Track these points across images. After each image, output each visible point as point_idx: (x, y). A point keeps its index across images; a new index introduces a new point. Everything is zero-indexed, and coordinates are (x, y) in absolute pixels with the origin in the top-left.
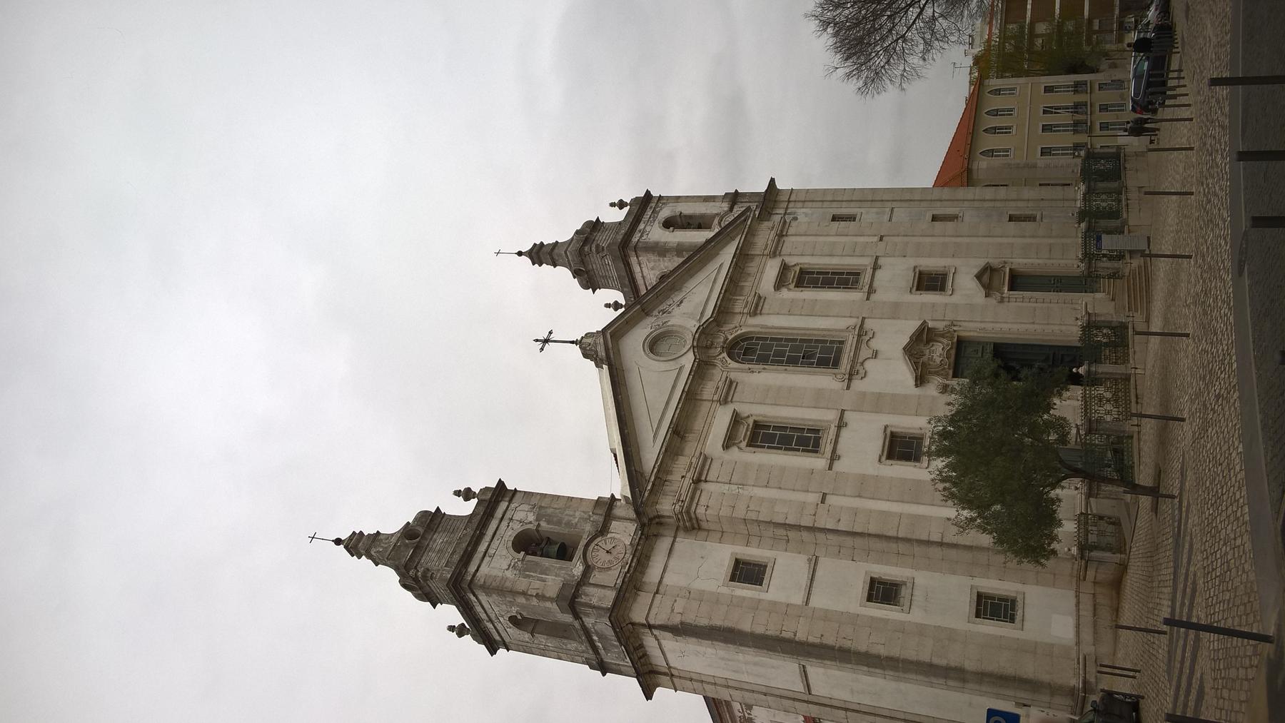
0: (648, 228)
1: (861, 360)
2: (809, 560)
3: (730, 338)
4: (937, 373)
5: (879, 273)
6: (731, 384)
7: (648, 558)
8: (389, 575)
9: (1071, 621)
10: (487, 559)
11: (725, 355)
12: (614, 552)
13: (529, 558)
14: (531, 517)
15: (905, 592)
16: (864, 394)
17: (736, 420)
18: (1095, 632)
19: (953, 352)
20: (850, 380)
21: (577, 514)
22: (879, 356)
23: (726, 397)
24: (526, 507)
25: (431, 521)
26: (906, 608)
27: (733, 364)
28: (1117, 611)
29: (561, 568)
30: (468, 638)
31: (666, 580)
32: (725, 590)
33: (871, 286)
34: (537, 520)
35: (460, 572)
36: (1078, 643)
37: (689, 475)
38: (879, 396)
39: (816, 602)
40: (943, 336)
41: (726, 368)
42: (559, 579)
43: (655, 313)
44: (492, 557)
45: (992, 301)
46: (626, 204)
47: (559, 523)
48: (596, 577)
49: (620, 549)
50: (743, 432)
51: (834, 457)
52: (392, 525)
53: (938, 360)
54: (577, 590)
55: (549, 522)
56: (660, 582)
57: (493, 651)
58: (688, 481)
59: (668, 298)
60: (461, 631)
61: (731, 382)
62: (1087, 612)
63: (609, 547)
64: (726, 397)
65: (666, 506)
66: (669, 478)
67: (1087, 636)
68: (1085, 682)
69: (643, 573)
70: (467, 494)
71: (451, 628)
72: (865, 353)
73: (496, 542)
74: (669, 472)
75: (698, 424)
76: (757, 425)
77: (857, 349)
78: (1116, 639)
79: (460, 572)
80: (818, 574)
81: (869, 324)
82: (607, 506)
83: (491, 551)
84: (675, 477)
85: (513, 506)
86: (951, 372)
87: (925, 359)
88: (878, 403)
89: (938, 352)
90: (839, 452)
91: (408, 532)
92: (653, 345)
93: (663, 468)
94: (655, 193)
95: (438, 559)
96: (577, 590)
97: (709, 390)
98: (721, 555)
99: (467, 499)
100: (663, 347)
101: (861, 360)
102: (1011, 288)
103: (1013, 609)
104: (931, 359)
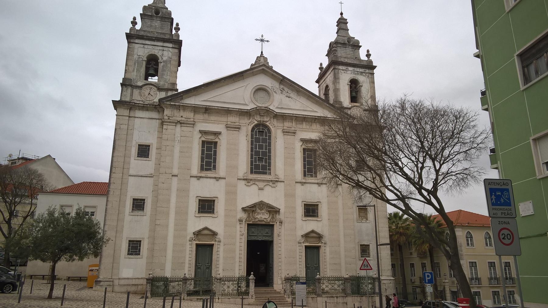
0: (349, 72)
1: (256, 183)
2: (151, 174)
3: (267, 124)
4: (249, 217)
5: (316, 186)
6: (238, 128)
7: (147, 110)
8: (333, 37)
9: (130, 276)
10: (142, 46)
11: (256, 122)
12: (150, 96)
13: (144, 63)
14: (165, 59)
15: (140, 213)
16: (236, 186)
17: (217, 134)
18: (124, 285)
19: (263, 223)
20: (244, 179)
21: (168, 77)
22: (260, 191)
23: (229, 127)
24: (170, 55)
25: (356, 46)
26: (132, 214)
27: (250, 128)
28: (135, 293)
29: (140, 77)
30: (319, 71)
31: (136, 120)
32: (134, 143)
33: (305, 183)
34: (164, 61)
35: (133, 37)
36: (119, 279)
37: (183, 119)
38: (235, 193)
39: (131, 179)
40: (273, 218)
41: (247, 126)
42: (135, 77)
43: (282, 86)
44: (143, 47)
45: (299, 238)
46: (369, 58)
47: (163, 70)
48: (136, 92)
49: (151, 98)
50: (211, 138)
51: (199, 178)
52: (352, 33)
53: (259, 217)
54: (129, 85)
55: (163, 66)
56: (135, 117)
57: (317, 82)
58: (179, 119)
59: (292, 90)
60: (321, 68)
61: (239, 128)
62: (134, 282)
63: (152, 93)
64: (229, 127)
65: (167, 112)
66: (181, 111)
67: (122, 282)
68: (100, 281)
69: (139, 110)
70: (368, 55)
71: (321, 64)
72: (261, 185)
73: (151, 47)
74: (184, 110)
75: (213, 118)
76: (216, 143)
77: (263, 181)
78: (124, 293)
79: (133, 37)
80: (145, 178)
81: (280, 186)
82: (177, 90)
83: (146, 46)
84: (182, 113)
85: (171, 49)
86: (251, 223)
87: (258, 211)
88: (231, 193)
89: (263, 216)
90: (201, 179)
91: (350, 39)
92: (261, 89)
93: (185, 107)
94: (375, 71)
95: (343, 53)
96: (129, 85)
97: (233, 119)
98: (150, 139)
99: (367, 56)
100: (261, 94)
101: (256, 183)
102: (306, 247)
103: (136, 254)
104: (258, 214)
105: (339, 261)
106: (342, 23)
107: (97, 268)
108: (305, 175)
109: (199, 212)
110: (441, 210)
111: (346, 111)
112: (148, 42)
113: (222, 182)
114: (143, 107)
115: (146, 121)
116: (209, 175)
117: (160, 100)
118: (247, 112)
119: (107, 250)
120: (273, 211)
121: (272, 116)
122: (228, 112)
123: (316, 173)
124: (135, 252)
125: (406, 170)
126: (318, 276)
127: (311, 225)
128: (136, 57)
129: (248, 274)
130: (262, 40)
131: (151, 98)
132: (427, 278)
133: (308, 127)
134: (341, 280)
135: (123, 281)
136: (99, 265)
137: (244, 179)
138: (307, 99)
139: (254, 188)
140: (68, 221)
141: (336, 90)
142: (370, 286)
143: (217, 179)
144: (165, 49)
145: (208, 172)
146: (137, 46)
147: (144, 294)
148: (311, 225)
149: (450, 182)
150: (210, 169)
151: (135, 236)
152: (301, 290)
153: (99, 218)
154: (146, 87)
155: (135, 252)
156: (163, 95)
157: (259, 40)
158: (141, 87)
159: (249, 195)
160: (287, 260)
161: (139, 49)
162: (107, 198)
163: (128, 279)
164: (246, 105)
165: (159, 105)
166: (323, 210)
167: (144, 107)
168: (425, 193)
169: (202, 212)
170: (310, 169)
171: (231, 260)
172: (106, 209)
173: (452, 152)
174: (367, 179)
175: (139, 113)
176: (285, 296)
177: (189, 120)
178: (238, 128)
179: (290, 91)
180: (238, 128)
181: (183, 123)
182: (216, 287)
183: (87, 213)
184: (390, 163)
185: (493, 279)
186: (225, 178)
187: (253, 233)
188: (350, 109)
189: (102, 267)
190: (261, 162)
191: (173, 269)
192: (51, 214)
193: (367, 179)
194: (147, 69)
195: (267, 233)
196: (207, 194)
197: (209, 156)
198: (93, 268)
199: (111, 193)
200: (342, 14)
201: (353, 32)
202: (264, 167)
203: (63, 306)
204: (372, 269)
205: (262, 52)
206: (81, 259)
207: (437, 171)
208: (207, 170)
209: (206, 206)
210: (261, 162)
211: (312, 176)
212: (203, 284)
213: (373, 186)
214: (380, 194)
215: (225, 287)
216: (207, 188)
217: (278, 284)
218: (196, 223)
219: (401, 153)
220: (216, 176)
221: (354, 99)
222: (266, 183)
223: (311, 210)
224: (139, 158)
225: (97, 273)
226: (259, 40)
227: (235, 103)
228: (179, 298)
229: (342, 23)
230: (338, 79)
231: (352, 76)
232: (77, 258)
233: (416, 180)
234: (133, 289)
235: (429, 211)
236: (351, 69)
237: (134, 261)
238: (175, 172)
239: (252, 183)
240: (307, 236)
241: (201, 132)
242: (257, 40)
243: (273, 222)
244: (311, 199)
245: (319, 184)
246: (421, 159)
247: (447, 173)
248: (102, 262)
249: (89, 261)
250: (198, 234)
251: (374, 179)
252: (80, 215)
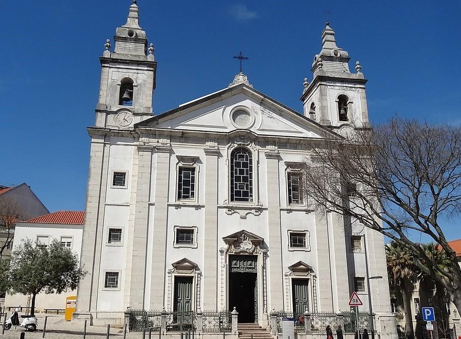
14: (139, 82)
15: (117, 243)
17: (196, 160)
21: (144, 101)
27: (230, 151)
41: (226, 151)
47: (138, 94)
49: (126, 123)
51: (178, 207)
76: (193, 170)
83: (120, 70)
89: (246, 246)
103: (113, 287)
105: (329, 297)
107: (75, 301)
108: (290, 202)
109: (177, 243)
110: (441, 240)
111: (335, 130)
116: (188, 203)
117: (136, 126)
119: (84, 283)
120: (259, 243)
123: (301, 199)
124: (112, 284)
125: (399, 195)
126: (307, 312)
127: (297, 256)
129: (231, 309)
130: (241, 58)
131: (126, 123)
132: (427, 315)
134: (333, 316)
136: (76, 298)
140: (46, 254)
141: (323, 108)
142: (366, 323)
143: (198, 207)
144: (139, 71)
147: (122, 328)
148: (297, 256)
149: (450, 208)
150: (188, 197)
152: (288, 327)
153: (75, 250)
155: (112, 284)
156: (138, 119)
157: (237, 58)
158: (115, 113)
159: (231, 225)
160: (273, 294)
162: (83, 228)
165: (134, 131)
166: (311, 240)
168: (422, 221)
169: (294, 246)
170: (295, 193)
171: (212, 294)
172: (83, 239)
173: (452, 174)
174: (357, 206)
176: (271, 333)
177: (165, 145)
182: (198, 323)
183: (62, 244)
184: (382, 189)
187: (235, 264)
188: (338, 128)
189: (80, 299)
190: (241, 188)
191: (152, 303)
192: (27, 245)
193: (357, 206)
194: (122, 93)
195: (250, 265)
196: (185, 224)
197: (187, 183)
199: (87, 223)
202: (246, 194)
204: (362, 304)
206: (59, 291)
207: (436, 196)
208: (185, 197)
209: (184, 235)
210: (241, 188)
211: (297, 202)
212: (182, 318)
213: (364, 212)
214: (372, 223)
215: (206, 322)
216: (184, 217)
217: (262, 320)
218: (177, 254)
219: (394, 176)
220: (196, 204)
221: (343, 117)
222: (249, 211)
223: (297, 239)
224: (115, 186)
225: (75, 306)
226: (237, 58)
228: (158, 333)
230: (326, 95)
231: (341, 92)
232: (55, 290)
233: (413, 206)
235: (426, 240)
237: (111, 293)
242: (235, 57)
243: (256, 253)
244: (298, 228)
245: (308, 211)
246: (417, 185)
247: (447, 198)
248: (80, 294)
249: (69, 293)
250: (178, 265)
251: (365, 205)
252: (58, 246)
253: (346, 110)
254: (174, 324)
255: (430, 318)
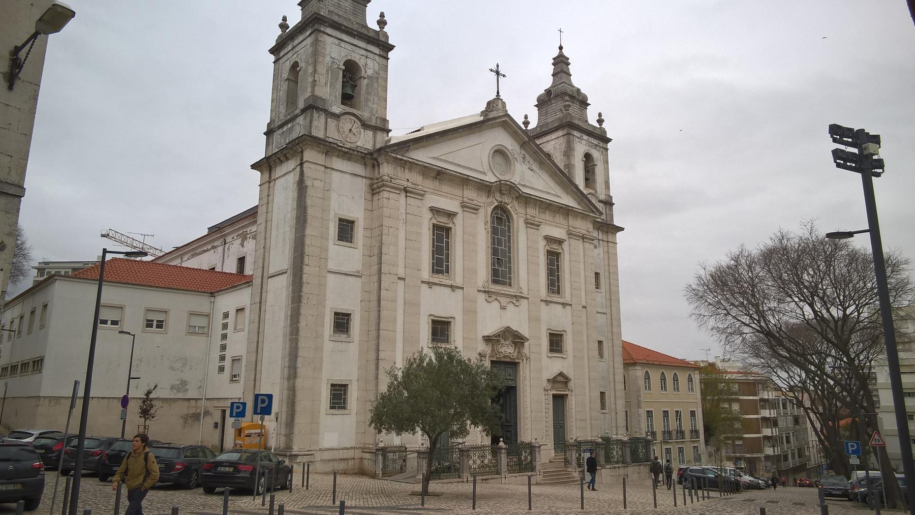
0: (584, 142)
1: (499, 298)
3: (509, 207)
4: (493, 350)
5: (560, 307)
7: (349, 159)
8: (547, 82)
9: (335, 444)
10: (337, 41)
11: (496, 204)
12: (351, 135)
15: (343, 337)
17: (451, 215)
18: (329, 461)
19: (508, 360)
20: (485, 292)
21: (375, 106)
24: (377, 68)
27: (490, 210)
28: (345, 473)
29: (336, 97)
33: (551, 302)
35: (325, 22)
36: (321, 450)
37: (409, 184)
41: (487, 205)
43: (523, 152)
44: (339, 45)
48: (332, 123)
49: (353, 139)
50: (443, 221)
51: (430, 284)
53: (502, 350)
54: (322, 110)
55: (367, 85)
61: (477, 210)
65: (386, 170)
66: (407, 170)
67: (327, 455)
68: (296, 456)
69: (338, 156)
72: (504, 301)
73: (349, 47)
74: (410, 169)
75: (446, 188)
77: (507, 296)
78: (327, 474)
79: (325, 22)
81: (524, 302)
83: (343, 44)
84: (407, 175)
85: (377, 57)
87: (502, 341)
88: (470, 312)
89: (507, 350)
92: (499, 152)
93: (412, 165)
96: (322, 110)
97: (470, 194)
98: (356, 211)
100: (499, 159)
101: (499, 298)
103: (339, 408)
104: (503, 346)
106: (561, 63)
107: (259, 431)
112: (344, 37)
113: (459, 292)
114: (347, 153)
115: (348, 177)
118: (487, 186)
121: (514, 196)
122: (464, 181)
124: (338, 403)
128: (328, 59)
132: (850, 449)
133: (551, 219)
135: (326, 453)
137: (485, 292)
138: (551, 176)
139: (496, 304)
144: (369, 55)
145: (440, 276)
146: (329, 40)
151: (339, 378)
154: (348, 116)
155: (338, 403)
158: (337, 117)
161: (333, 46)
163: (333, 449)
164: (484, 173)
167: (348, 154)
175: (338, 163)
178: (474, 209)
179: (532, 162)
180: (474, 209)
181: (411, 192)
185: (667, 433)
186: (463, 288)
198: (252, 431)
200: (561, 48)
201: (579, 79)
203: (658, 509)
205: (498, 93)
227: (471, 169)
229: (561, 63)
234: (341, 466)
236: (585, 137)
238: (401, 272)
239: (494, 297)
240: (553, 381)
241: (433, 210)
253: (354, 87)
254: (755, 455)
255: (854, 452)
